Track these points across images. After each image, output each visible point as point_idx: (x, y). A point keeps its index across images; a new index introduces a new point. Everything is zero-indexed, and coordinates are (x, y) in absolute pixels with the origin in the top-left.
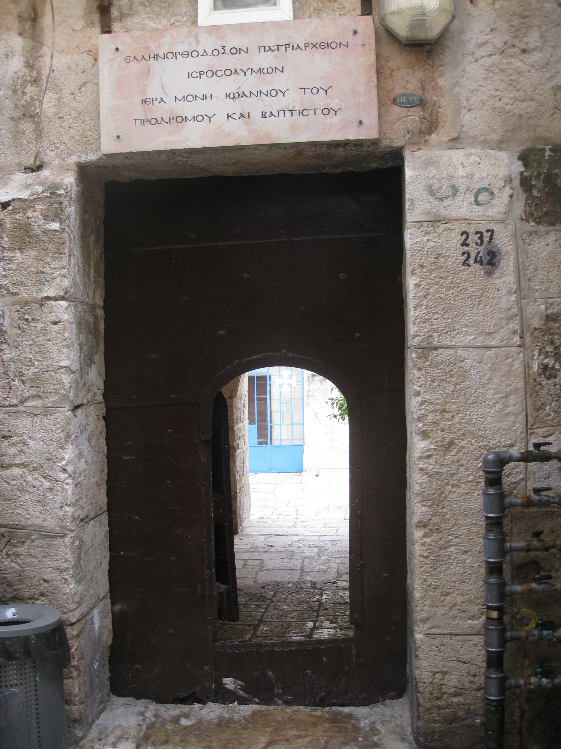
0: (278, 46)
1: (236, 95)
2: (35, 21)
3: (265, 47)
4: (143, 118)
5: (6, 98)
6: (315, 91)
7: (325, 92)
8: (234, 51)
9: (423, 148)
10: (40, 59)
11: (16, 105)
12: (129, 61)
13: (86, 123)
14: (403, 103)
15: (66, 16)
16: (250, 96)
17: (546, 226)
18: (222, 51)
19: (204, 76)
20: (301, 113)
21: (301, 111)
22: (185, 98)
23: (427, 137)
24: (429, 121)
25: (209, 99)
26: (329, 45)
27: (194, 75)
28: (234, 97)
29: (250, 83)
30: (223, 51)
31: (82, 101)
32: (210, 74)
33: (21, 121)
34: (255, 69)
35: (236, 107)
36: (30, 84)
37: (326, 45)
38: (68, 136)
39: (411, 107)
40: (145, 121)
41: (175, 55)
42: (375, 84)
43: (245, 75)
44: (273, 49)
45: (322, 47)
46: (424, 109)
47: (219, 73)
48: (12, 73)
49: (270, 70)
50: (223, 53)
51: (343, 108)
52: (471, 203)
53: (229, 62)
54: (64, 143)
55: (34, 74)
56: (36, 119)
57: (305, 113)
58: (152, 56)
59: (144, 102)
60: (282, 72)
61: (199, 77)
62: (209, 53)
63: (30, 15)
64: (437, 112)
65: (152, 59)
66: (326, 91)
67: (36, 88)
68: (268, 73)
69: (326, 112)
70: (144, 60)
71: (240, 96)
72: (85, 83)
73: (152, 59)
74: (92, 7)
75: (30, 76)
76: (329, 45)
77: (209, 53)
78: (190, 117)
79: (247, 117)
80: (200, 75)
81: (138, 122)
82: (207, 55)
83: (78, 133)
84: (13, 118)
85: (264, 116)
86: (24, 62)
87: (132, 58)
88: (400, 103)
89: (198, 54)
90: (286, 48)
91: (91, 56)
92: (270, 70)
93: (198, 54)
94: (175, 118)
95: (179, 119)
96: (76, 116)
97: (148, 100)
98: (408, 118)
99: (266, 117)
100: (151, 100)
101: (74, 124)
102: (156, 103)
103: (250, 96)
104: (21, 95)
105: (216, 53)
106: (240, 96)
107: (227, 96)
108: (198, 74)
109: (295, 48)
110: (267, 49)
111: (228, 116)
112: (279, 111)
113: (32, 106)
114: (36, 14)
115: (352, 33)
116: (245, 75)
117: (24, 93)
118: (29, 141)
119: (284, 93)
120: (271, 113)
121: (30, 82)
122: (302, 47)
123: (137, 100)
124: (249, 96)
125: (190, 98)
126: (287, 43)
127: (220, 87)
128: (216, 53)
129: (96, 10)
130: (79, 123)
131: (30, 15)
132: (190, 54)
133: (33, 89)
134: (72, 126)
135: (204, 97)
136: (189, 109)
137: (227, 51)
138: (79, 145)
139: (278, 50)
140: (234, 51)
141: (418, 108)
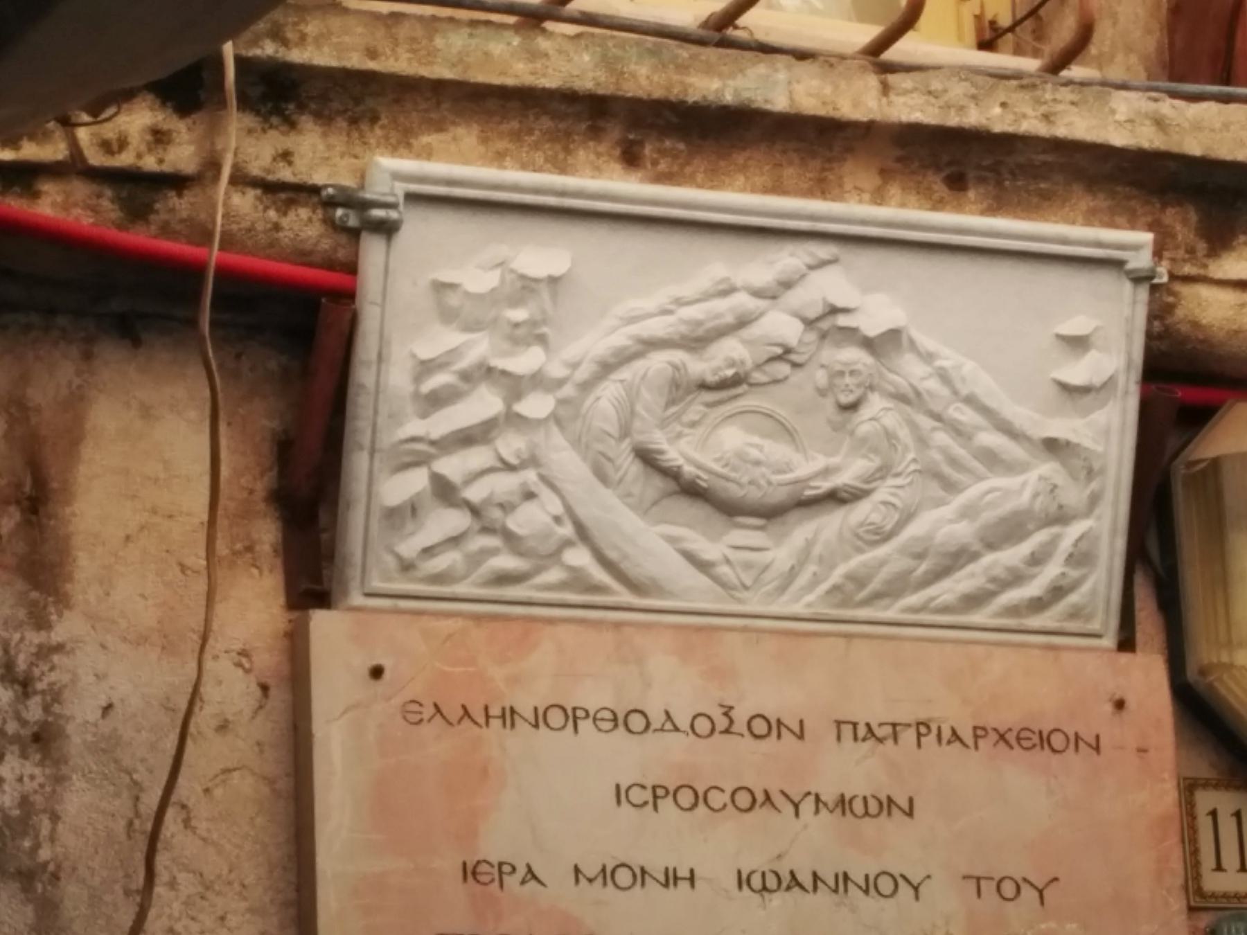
0: (894, 725)
1: (771, 882)
3: (855, 725)
7: (1036, 894)
10: (56, 658)
12: (416, 718)
15: (154, 511)
16: (815, 888)
18: (722, 723)
19: (666, 805)
22: (607, 875)
25: (684, 886)
26: (1045, 740)
27: (637, 796)
28: (765, 888)
31: (215, 836)
32: (686, 798)
34: (829, 796)
36: (15, 748)
37: (1036, 739)
42: (1179, 881)
44: (880, 732)
45: (1025, 744)
47: (717, 799)
49: (873, 807)
50: (727, 731)
52: (779, 857)
53: (748, 762)
55: (34, 711)
56: (39, 887)
58: (495, 711)
59: (470, 872)
61: (650, 806)
63: (19, 486)
65: (496, 723)
66: (1041, 892)
67: (41, 764)
68: (867, 813)
70: (466, 722)
71: (784, 885)
72: (227, 771)
73: (496, 723)
76: (1045, 740)
80: (655, 797)
82: (677, 729)
87: (428, 711)
89: (648, 725)
90: (919, 735)
92: (873, 807)
93: (648, 725)
101: (185, 921)
102: (512, 881)
103: (815, 888)
106: (784, 885)
107: (743, 881)
108: (648, 795)
109: (944, 741)
110: (862, 731)
113: (24, 834)
114: (40, 482)
116: (797, 814)
119: (916, 889)
121: (16, 739)
122: (967, 736)
123: (449, 864)
124: (810, 888)
125: (624, 877)
126: (922, 716)
128: (703, 726)
131: (19, 486)
132: (621, 721)
135: (670, 879)
137: (740, 726)
139: (896, 740)
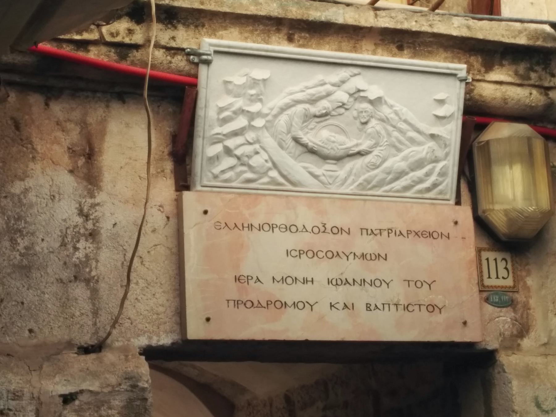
0: (380, 230)
1: (339, 282)
2: (90, 158)
4: (237, 299)
5: (50, 252)
6: (419, 284)
7: (428, 286)
8: (335, 230)
9: (516, 352)
10: (97, 208)
11: (65, 263)
12: (219, 227)
13: (157, 296)
14: (496, 303)
16: (354, 284)
17: (243, 390)
18: (322, 229)
19: (304, 256)
20: (406, 308)
21: (406, 306)
23: (519, 341)
24: (520, 324)
26: (431, 235)
27: (293, 253)
28: (337, 284)
29: (353, 269)
30: (323, 228)
32: (310, 254)
33: (72, 284)
34: (358, 254)
35: (339, 295)
36: (83, 238)
37: (428, 234)
38: (135, 311)
39: (503, 307)
40: (239, 302)
41: (272, 227)
43: (348, 260)
44: (375, 232)
46: (515, 311)
47: (321, 255)
48: (61, 221)
50: (324, 232)
51: (447, 305)
54: (129, 319)
55: (90, 225)
57: (410, 308)
58: (246, 225)
60: (386, 259)
61: (298, 257)
62: (309, 229)
64: (528, 314)
65: (246, 229)
69: (430, 308)
70: (236, 229)
71: (344, 283)
73: (246, 229)
74: (163, 152)
75: (85, 227)
76: (431, 235)
77: (309, 229)
78: (290, 303)
79: (351, 308)
80: (300, 254)
81: (231, 303)
82: (307, 231)
83: (148, 308)
84: (61, 279)
85: (368, 309)
86: (76, 208)
87: (223, 225)
88: (493, 302)
89: (297, 230)
90: (389, 233)
91: (162, 212)
94: (273, 302)
95: (278, 305)
96: (144, 285)
97: (243, 278)
98: (501, 318)
99: (371, 310)
100: (246, 279)
102: (252, 282)
103: (354, 284)
104: (71, 250)
105: (316, 230)
106: (344, 283)
107: (330, 282)
108: (297, 253)
110: (369, 232)
111: (331, 306)
112: (383, 304)
113: (87, 267)
114: (92, 149)
115: (452, 224)
116: (348, 260)
117: (76, 249)
118: (83, 311)
119: (388, 284)
120: (376, 306)
121: (84, 235)
122: (405, 233)
124: (352, 284)
125: (289, 280)
126: (390, 227)
127: (322, 271)
128: (316, 230)
129: (167, 157)
130: (149, 296)
131: (84, 150)
133: (88, 245)
134: (139, 298)
135: (305, 281)
136: (290, 293)
137: (328, 230)
138: (149, 323)
140: (335, 230)
141: (509, 308)
